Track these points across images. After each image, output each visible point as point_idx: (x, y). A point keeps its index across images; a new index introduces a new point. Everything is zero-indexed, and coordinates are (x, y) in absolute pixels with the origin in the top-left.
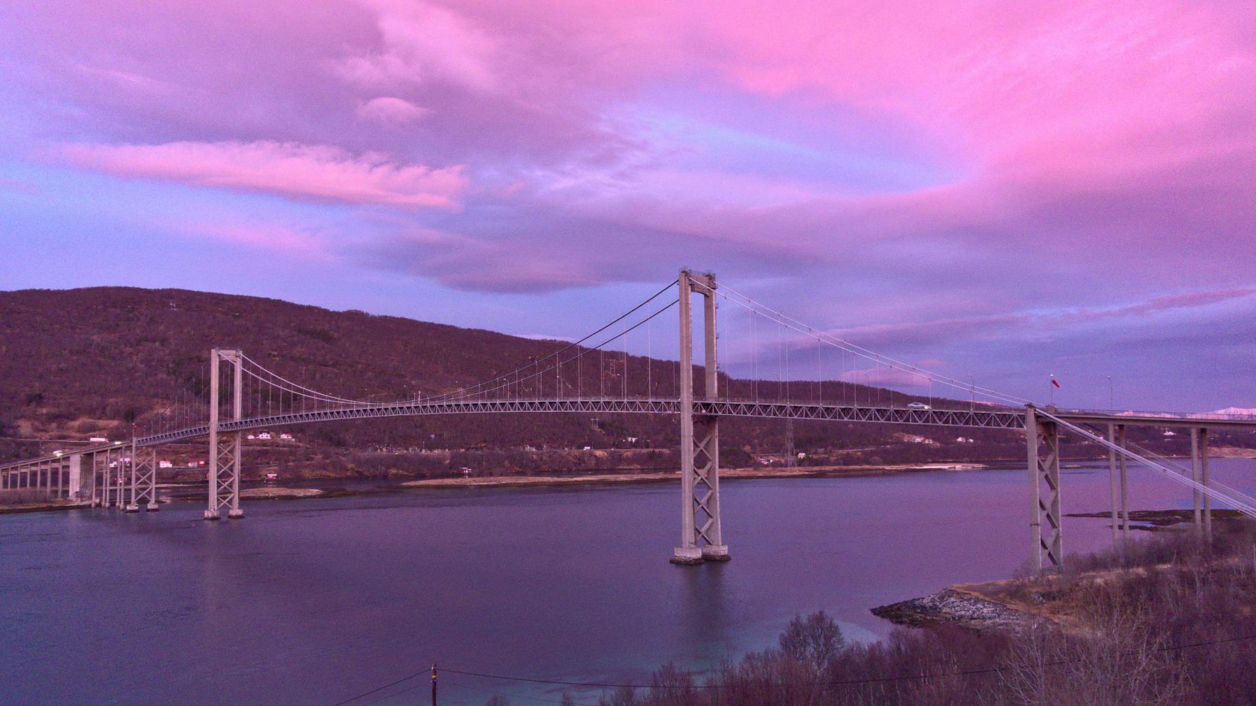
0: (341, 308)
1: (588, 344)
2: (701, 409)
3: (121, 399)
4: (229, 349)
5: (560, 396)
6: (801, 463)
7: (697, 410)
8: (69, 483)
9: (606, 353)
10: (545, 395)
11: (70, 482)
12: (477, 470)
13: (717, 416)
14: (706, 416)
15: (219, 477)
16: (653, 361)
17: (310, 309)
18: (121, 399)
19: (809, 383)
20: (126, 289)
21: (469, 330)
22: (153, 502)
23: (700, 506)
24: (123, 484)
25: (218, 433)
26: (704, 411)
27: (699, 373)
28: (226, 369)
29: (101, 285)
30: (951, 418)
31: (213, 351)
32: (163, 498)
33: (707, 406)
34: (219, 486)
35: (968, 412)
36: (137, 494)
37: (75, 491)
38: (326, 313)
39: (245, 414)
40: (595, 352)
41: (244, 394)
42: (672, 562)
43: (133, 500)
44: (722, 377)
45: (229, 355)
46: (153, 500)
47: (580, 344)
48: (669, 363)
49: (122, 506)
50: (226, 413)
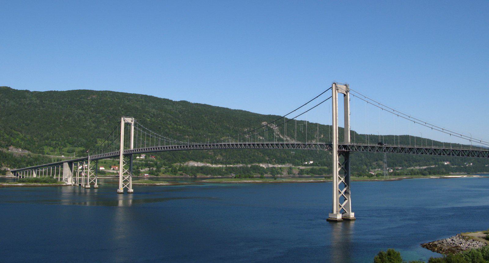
0: (178, 100)
1: (289, 117)
2: (342, 148)
3: (84, 125)
4: (129, 118)
5: (275, 141)
6: (390, 174)
7: (340, 149)
8: (63, 175)
9: (298, 121)
10: (269, 140)
11: (63, 175)
12: (238, 175)
13: (350, 151)
14: (345, 151)
15: (124, 174)
16: (452, 144)
17: (165, 100)
18: (84, 125)
19: (393, 136)
20: (227, 109)
21: (257, 114)
22: (96, 184)
23: (341, 194)
24: (84, 176)
25: (123, 155)
26: (343, 149)
27: (342, 131)
28: (127, 125)
29: (225, 107)
30: (461, 153)
31: (122, 118)
32: (101, 183)
33: (345, 147)
34: (123, 178)
35: (479, 150)
36: (90, 181)
37: (65, 178)
38: (230, 110)
39: (134, 147)
40: (292, 121)
41: (135, 137)
42: (328, 220)
43: (88, 183)
44: (352, 133)
45: (129, 120)
46: (96, 184)
47: (286, 117)
48: (328, 126)
49: (84, 186)
50: (127, 145)
